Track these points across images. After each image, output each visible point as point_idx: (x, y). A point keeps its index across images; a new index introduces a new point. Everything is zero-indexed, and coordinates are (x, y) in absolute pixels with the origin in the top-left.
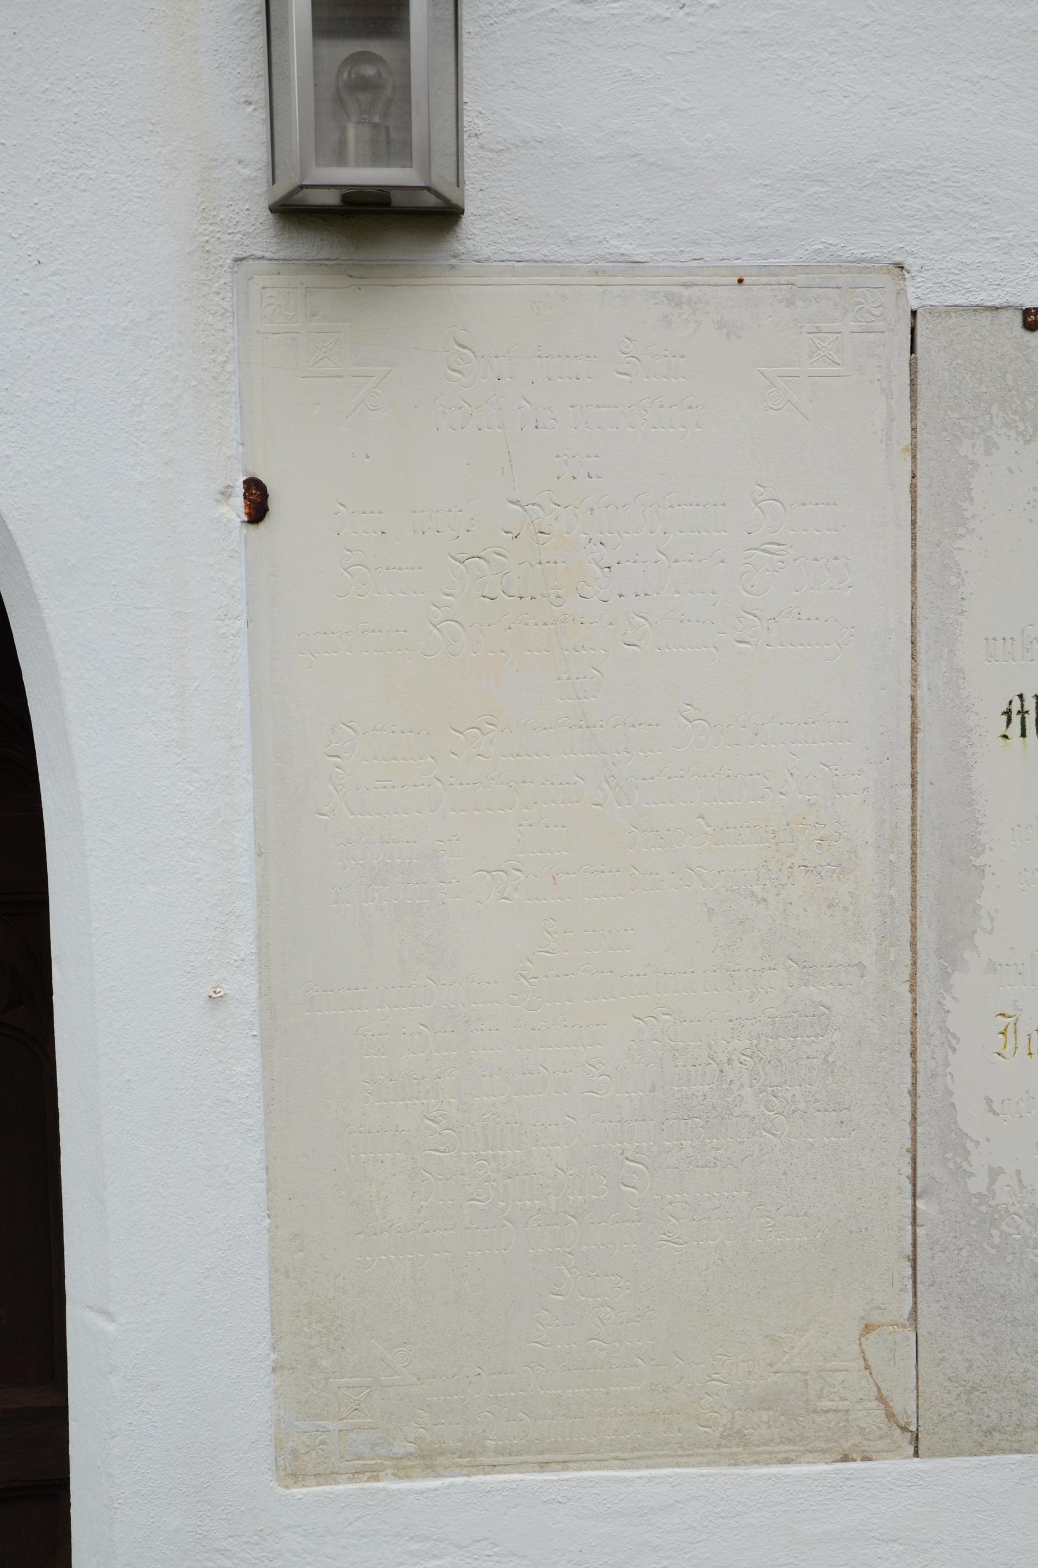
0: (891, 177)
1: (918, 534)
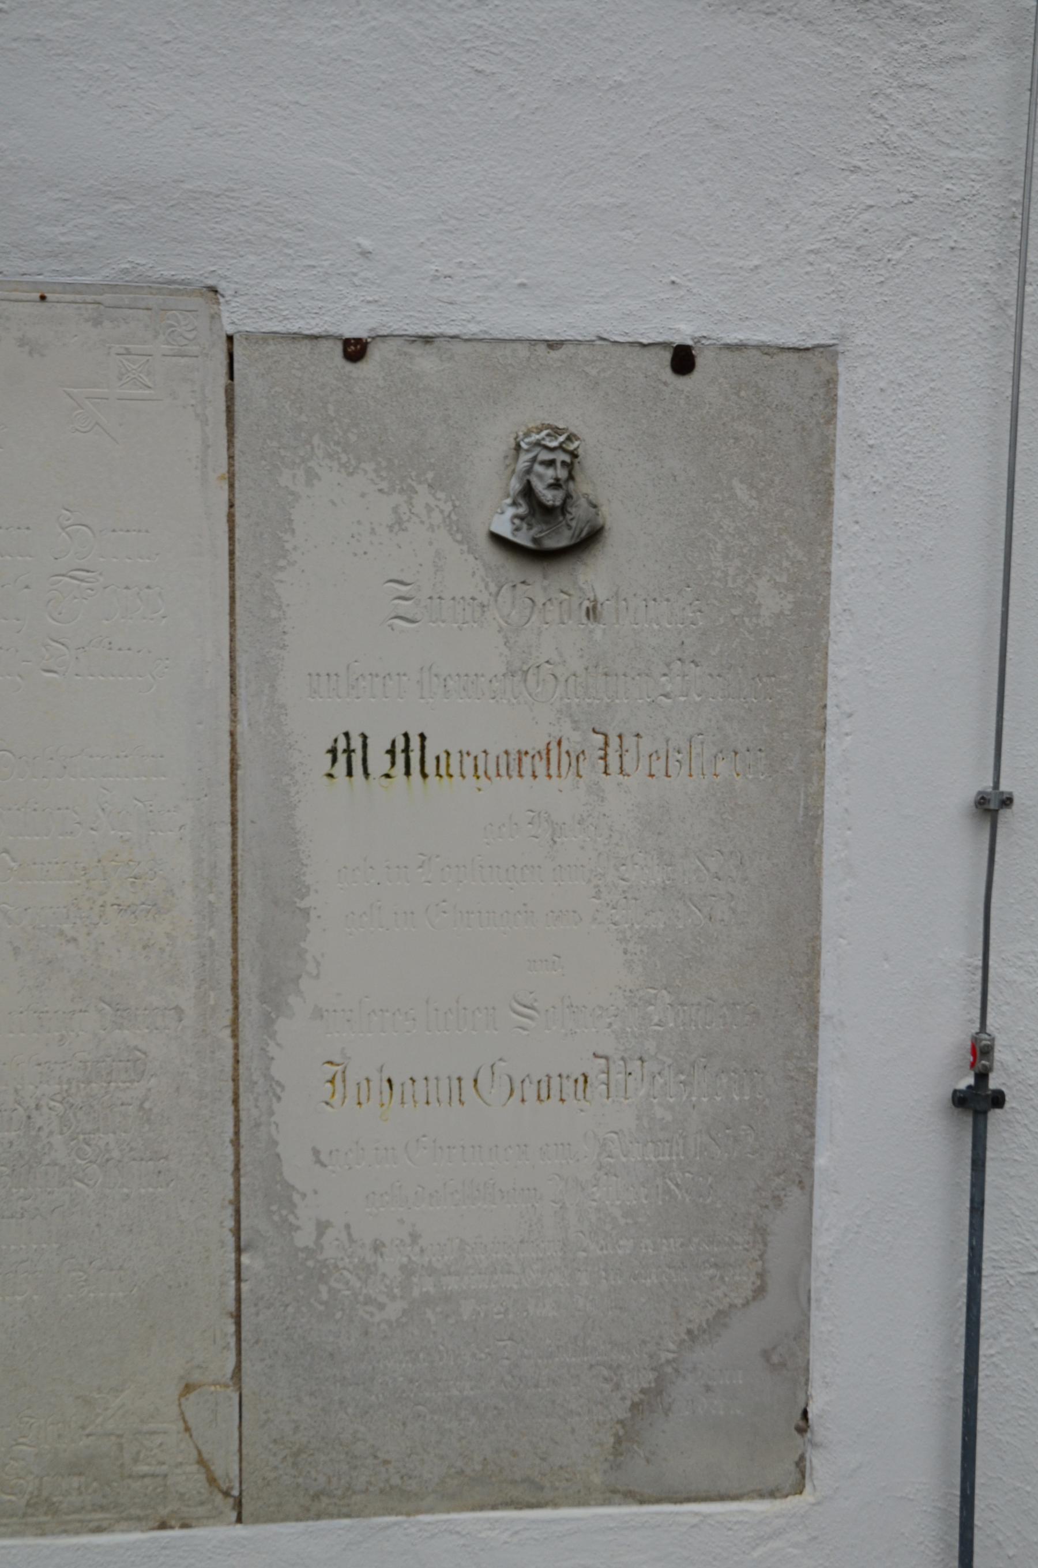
0: (198, 199)
1: (237, 565)
